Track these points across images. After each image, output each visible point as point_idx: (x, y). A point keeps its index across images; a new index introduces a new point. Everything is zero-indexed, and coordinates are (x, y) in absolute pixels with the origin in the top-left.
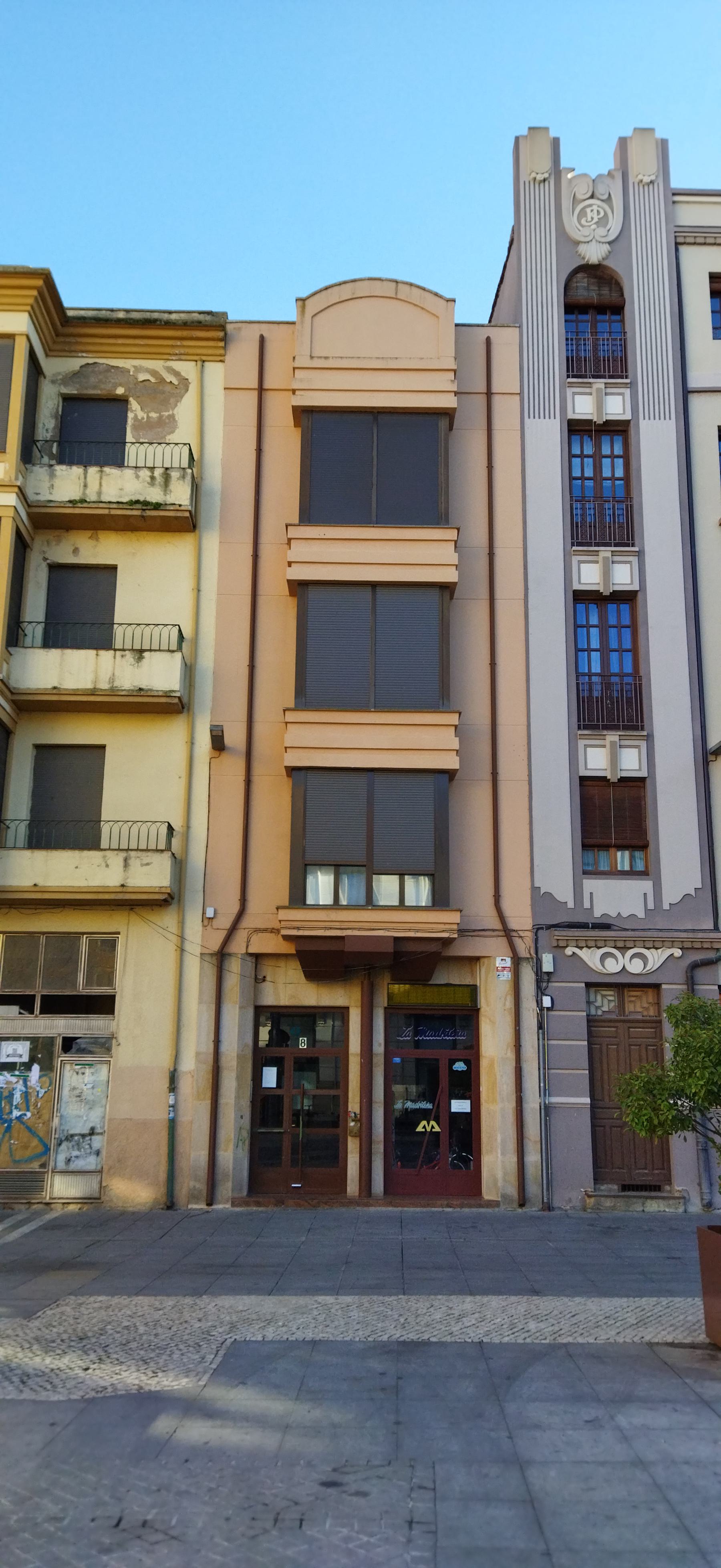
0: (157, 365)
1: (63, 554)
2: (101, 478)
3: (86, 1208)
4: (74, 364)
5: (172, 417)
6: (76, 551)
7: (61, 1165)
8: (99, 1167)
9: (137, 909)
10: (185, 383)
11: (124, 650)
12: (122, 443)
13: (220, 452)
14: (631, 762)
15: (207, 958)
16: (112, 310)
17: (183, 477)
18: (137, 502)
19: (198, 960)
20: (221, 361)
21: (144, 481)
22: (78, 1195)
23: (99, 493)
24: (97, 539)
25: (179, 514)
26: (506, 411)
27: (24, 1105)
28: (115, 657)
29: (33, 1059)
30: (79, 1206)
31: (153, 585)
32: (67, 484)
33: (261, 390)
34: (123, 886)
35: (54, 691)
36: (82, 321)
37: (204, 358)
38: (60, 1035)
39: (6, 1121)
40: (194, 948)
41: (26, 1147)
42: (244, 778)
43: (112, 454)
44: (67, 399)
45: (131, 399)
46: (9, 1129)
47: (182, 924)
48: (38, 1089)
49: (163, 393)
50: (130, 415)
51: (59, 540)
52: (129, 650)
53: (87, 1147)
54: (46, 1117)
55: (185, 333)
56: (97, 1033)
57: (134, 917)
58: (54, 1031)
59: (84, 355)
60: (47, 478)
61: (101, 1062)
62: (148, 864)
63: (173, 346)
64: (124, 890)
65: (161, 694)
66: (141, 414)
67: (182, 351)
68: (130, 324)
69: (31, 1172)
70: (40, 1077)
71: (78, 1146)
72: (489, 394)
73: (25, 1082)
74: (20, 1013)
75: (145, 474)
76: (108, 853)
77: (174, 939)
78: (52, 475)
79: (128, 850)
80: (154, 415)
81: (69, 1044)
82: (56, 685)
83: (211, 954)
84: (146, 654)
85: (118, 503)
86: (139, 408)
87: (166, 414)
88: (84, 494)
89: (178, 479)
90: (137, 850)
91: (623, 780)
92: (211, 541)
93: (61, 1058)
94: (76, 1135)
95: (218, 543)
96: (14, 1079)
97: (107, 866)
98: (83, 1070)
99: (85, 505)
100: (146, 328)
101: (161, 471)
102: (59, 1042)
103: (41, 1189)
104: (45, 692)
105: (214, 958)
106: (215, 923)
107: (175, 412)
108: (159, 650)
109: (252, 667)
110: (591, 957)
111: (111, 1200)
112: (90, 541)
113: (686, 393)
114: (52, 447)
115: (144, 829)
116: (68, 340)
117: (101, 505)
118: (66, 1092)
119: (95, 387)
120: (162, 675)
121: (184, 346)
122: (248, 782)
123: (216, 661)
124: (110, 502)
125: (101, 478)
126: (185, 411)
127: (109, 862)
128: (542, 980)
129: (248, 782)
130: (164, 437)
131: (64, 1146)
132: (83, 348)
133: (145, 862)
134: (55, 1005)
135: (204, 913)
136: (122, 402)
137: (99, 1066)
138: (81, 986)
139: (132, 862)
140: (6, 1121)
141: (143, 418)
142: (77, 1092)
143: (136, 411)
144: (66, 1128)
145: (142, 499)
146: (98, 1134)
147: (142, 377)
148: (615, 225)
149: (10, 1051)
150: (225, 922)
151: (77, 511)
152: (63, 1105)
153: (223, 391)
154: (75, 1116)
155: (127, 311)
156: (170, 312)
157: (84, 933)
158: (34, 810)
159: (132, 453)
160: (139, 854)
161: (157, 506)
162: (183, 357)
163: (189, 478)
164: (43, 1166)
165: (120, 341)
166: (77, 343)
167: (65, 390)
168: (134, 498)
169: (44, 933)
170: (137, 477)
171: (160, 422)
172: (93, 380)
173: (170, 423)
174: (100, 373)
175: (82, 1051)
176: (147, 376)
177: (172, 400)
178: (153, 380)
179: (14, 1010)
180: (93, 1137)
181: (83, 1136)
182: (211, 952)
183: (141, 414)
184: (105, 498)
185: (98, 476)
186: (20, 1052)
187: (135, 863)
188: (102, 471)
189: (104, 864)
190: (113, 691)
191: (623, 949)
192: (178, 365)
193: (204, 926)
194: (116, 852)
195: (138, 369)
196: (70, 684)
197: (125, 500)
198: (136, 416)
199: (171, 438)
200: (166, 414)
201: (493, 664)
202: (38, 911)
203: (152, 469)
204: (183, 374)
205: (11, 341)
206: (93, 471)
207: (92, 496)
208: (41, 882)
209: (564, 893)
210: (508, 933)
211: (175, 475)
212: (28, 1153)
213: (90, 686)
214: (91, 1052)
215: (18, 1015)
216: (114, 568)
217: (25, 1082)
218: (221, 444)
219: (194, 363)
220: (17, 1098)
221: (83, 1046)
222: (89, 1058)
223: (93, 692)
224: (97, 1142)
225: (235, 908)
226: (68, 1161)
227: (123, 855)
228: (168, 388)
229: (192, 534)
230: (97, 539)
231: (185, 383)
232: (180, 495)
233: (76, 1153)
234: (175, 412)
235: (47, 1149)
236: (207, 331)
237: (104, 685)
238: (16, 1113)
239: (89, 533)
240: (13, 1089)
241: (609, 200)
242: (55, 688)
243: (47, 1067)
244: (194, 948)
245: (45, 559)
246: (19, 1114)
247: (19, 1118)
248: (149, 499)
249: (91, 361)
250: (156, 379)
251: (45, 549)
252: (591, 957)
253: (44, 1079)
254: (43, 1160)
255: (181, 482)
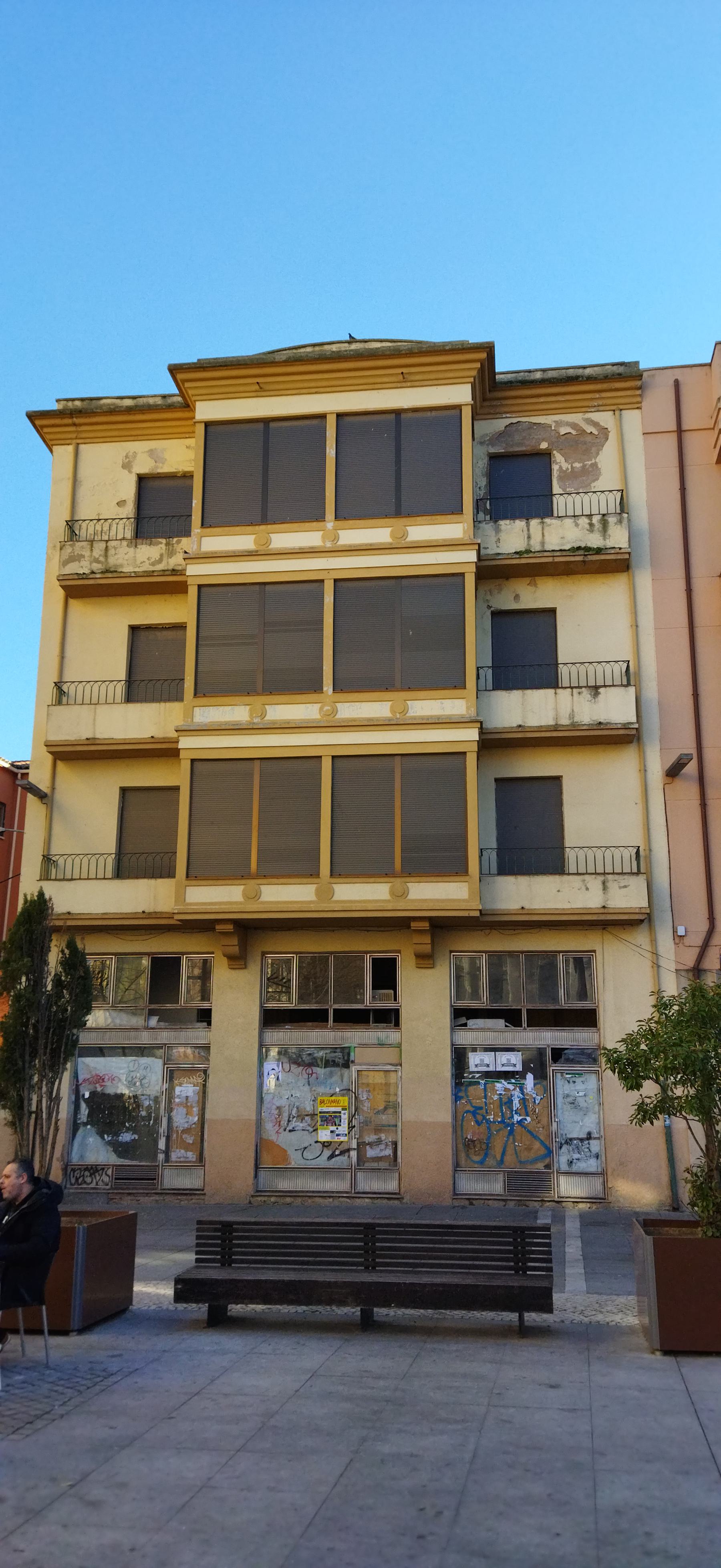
0: (576, 418)
1: (506, 601)
2: (543, 529)
3: (594, 1207)
4: (500, 424)
5: (595, 465)
6: (517, 597)
7: (564, 1167)
8: (600, 1170)
9: (610, 928)
10: (604, 432)
11: (579, 687)
12: (549, 495)
13: (645, 494)
15: (683, 973)
16: (530, 371)
17: (620, 521)
18: (579, 548)
19: (674, 975)
20: (638, 408)
21: (583, 528)
22: (583, 1195)
23: (543, 543)
24: (535, 585)
25: (619, 557)
27: (523, 1110)
28: (572, 695)
29: (526, 1068)
30: (588, 1205)
31: (593, 624)
32: (513, 537)
33: (680, 431)
34: (604, 907)
35: (520, 729)
36: (510, 385)
37: (621, 407)
38: (548, 1046)
39: (508, 1125)
40: (669, 962)
41: (529, 1149)
42: (699, 802)
43: (539, 505)
44: (493, 457)
45: (555, 452)
46: (511, 1132)
47: (654, 941)
48: (534, 1096)
49: (585, 444)
50: (555, 468)
51: (500, 590)
52: (585, 687)
53: (587, 1150)
54: (545, 1120)
55: (605, 386)
56: (583, 1044)
57: (608, 937)
58: (542, 1043)
59: (508, 415)
60: (494, 533)
61: (591, 1072)
62: (625, 887)
63: (592, 399)
64: (606, 911)
65: (619, 726)
66: (565, 466)
67: (601, 403)
68: (553, 383)
69: (536, 1173)
70: (535, 1085)
71: (578, 1149)
73: (521, 1089)
74: (506, 1026)
75: (584, 521)
76: (587, 877)
77: (648, 955)
78: (498, 530)
79: (604, 874)
80: (577, 465)
81: (558, 1054)
82: (520, 723)
83: (687, 971)
84: (601, 690)
85: (561, 550)
86: (563, 459)
87: (590, 463)
88: (528, 544)
89: (616, 524)
90: (613, 873)
92: (644, 579)
93: (552, 1068)
94: (575, 1139)
95: (651, 581)
96: (511, 1087)
97: (587, 889)
98: (574, 1079)
99: (531, 555)
100: (568, 385)
101: (599, 517)
102: (549, 1053)
103: (549, 1189)
104: (510, 730)
105: (691, 974)
106: (687, 941)
107: (597, 460)
108: (613, 686)
109: (696, 695)
111: (619, 1201)
112: (529, 587)
114: (485, 504)
115: (608, 854)
116: (495, 403)
117: (546, 554)
118: (560, 1100)
119: (521, 444)
120: (616, 707)
121: (604, 398)
122: (704, 805)
123: (660, 691)
124: (553, 551)
125: (543, 529)
126: (607, 458)
127: (589, 885)
129: (704, 805)
130: (589, 485)
131: (565, 1147)
132: (506, 409)
133: (622, 885)
134: (542, 1019)
135: (675, 931)
136: (547, 455)
137: (587, 1076)
138: (565, 1000)
139: (610, 884)
140: (508, 1125)
141: (568, 469)
142: (570, 1099)
143: (560, 462)
144: (566, 1132)
145: (583, 545)
146: (595, 1138)
147: (563, 431)
149: (504, 1061)
150: (697, 940)
151: (523, 561)
152: (560, 1112)
153: (641, 437)
154: (573, 1124)
155: (544, 371)
156: (584, 367)
157: (560, 952)
158: (499, 840)
159: (559, 503)
160: (616, 877)
161: (599, 551)
162: (601, 408)
163: (625, 522)
164: (548, 1166)
165: (542, 400)
166: (502, 405)
167: (492, 450)
168: (576, 545)
169: (522, 952)
170: (577, 525)
171: (584, 471)
172: (517, 438)
173: (593, 472)
174: (524, 430)
175: (569, 1061)
176: (568, 430)
177: (594, 449)
178: (574, 432)
179: (501, 1023)
180: (591, 1142)
181: (582, 1140)
182: (686, 968)
183: (565, 466)
184: (548, 547)
185: (540, 527)
186: (513, 1061)
187: (613, 886)
188: (543, 523)
189: (584, 888)
190: (574, 726)
192: (596, 416)
193: (675, 944)
194: (594, 876)
195: (558, 424)
196: (533, 721)
197: (567, 547)
198: (561, 467)
199: (598, 485)
200: (590, 463)
202: (516, 932)
203: (590, 516)
204: (602, 424)
205: (457, 412)
206: (534, 523)
207: (536, 546)
208: (527, 906)
211: (612, 520)
212: (532, 1155)
213: (551, 722)
214: (580, 1062)
215: (504, 1027)
216: (552, 611)
217: (521, 1089)
218: (644, 486)
219: (611, 413)
220: (516, 1104)
221: (571, 1057)
222: (578, 1067)
223: (556, 728)
224: (595, 1146)
225: (704, 926)
226: (570, 1163)
227: (601, 878)
228: (589, 439)
229: (626, 574)
230: (535, 585)
231: (604, 432)
232: (618, 538)
233: (576, 1156)
234: (597, 460)
235: (550, 1152)
236: (621, 382)
237: (565, 721)
238: (517, 1118)
239: (528, 580)
240: (512, 1096)
242: (520, 726)
243: (541, 1075)
244: (669, 962)
245: (489, 607)
246: (519, 1118)
247: (520, 1123)
248: (589, 545)
249: (515, 420)
250: (577, 431)
251: (489, 597)
253: (538, 1086)
254: (547, 1161)
255: (619, 527)
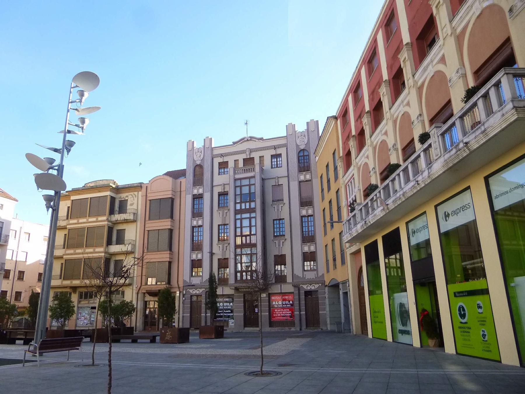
14: (312, 248)
26: (183, 194)
72: (181, 191)
91: (198, 260)
92: (139, 223)
110: (191, 291)
113: (288, 176)
128: (184, 295)
148: (202, 157)
150: (139, 288)
191: (311, 285)
201: (291, 231)
209: (188, 280)
210: (179, 288)
241: (201, 152)
252: (191, 291)
